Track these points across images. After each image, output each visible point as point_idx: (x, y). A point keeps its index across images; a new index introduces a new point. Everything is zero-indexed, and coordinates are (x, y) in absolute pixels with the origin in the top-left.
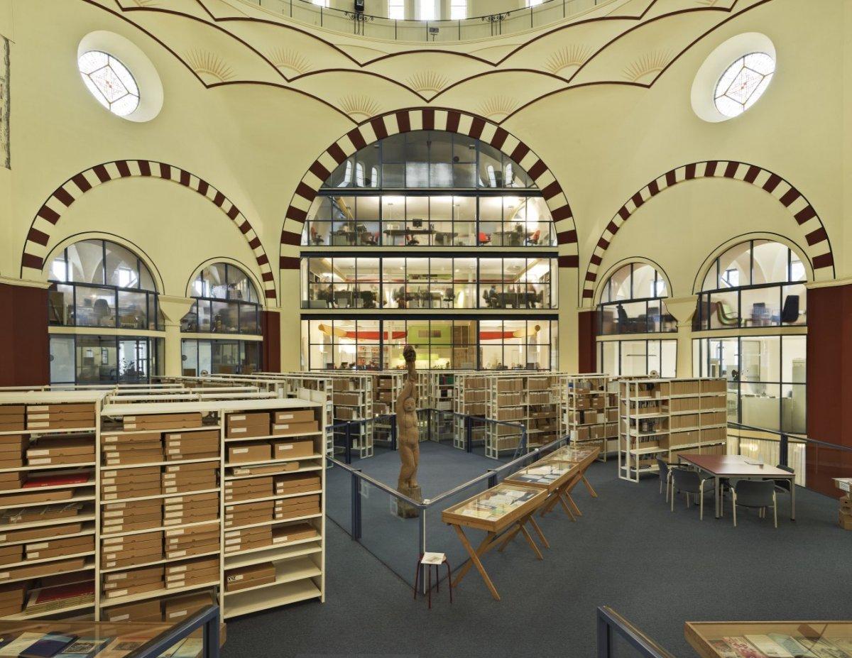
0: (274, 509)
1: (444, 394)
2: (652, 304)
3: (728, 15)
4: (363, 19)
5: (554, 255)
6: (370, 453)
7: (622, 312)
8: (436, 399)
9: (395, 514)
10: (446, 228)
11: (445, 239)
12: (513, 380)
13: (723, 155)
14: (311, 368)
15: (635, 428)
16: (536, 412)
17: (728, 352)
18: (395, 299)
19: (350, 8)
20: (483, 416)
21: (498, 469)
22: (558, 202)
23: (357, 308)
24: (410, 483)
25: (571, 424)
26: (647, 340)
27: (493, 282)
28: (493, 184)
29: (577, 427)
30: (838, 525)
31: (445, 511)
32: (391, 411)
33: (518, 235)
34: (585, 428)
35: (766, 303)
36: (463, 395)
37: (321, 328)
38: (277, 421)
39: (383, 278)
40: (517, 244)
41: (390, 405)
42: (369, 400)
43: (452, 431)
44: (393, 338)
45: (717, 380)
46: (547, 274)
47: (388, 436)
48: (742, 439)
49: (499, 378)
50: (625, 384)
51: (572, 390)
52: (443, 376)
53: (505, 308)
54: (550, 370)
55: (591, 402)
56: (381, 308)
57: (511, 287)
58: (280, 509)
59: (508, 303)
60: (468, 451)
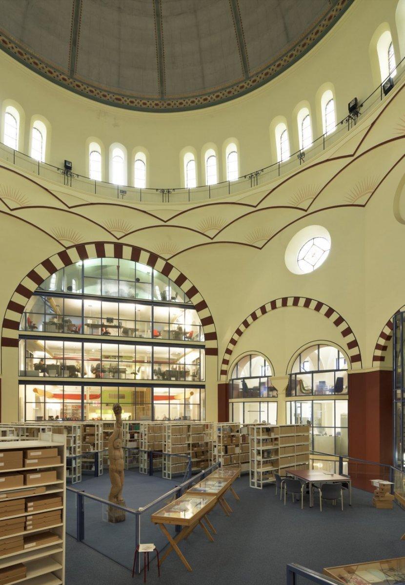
0: (25, 523)
1: (132, 436)
2: (264, 380)
3: (304, 213)
4: (71, 176)
5: (202, 347)
6: (79, 480)
7: (245, 385)
8: (127, 441)
9: (106, 520)
10: (130, 325)
11: (130, 332)
12: (181, 426)
13: (304, 294)
14: (27, 419)
15: (260, 456)
16: (195, 447)
17: (306, 410)
18: (92, 372)
19: (62, 167)
20: (161, 451)
21: (182, 485)
22: (205, 313)
23: (63, 377)
24: (117, 498)
25: (219, 454)
26: (260, 402)
27: (160, 363)
28: (160, 298)
29: (223, 456)
30: (373, 506)
31: (153, 515)
32: (94, 449)
33: (179, 333)
34: (228, 456)
35: (326, 381)
36: (146, 437)
37: (35, 390)
38: (29, 457)
39: (85, 357)
40: (178, 339)
41: (94, 445)
42: (79, 442)
43: (138, 462)
44: (90, 399)
45: (298, 426)
46: (197, 359)
47: (91, 467)
48: (315, 461)
49: (172, 426)
50: (254, 429)
51: (220, 433)
52: (131, 425)
53: (170, 380)
54: (200, 420)
55: (232, 440)
56: (82, 377)
57: (175, 366)
58: (30, 522)
59: (173, 377)
60: (150, 475)
